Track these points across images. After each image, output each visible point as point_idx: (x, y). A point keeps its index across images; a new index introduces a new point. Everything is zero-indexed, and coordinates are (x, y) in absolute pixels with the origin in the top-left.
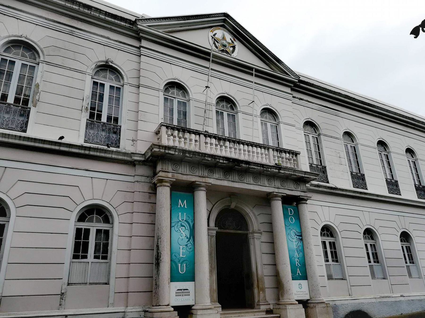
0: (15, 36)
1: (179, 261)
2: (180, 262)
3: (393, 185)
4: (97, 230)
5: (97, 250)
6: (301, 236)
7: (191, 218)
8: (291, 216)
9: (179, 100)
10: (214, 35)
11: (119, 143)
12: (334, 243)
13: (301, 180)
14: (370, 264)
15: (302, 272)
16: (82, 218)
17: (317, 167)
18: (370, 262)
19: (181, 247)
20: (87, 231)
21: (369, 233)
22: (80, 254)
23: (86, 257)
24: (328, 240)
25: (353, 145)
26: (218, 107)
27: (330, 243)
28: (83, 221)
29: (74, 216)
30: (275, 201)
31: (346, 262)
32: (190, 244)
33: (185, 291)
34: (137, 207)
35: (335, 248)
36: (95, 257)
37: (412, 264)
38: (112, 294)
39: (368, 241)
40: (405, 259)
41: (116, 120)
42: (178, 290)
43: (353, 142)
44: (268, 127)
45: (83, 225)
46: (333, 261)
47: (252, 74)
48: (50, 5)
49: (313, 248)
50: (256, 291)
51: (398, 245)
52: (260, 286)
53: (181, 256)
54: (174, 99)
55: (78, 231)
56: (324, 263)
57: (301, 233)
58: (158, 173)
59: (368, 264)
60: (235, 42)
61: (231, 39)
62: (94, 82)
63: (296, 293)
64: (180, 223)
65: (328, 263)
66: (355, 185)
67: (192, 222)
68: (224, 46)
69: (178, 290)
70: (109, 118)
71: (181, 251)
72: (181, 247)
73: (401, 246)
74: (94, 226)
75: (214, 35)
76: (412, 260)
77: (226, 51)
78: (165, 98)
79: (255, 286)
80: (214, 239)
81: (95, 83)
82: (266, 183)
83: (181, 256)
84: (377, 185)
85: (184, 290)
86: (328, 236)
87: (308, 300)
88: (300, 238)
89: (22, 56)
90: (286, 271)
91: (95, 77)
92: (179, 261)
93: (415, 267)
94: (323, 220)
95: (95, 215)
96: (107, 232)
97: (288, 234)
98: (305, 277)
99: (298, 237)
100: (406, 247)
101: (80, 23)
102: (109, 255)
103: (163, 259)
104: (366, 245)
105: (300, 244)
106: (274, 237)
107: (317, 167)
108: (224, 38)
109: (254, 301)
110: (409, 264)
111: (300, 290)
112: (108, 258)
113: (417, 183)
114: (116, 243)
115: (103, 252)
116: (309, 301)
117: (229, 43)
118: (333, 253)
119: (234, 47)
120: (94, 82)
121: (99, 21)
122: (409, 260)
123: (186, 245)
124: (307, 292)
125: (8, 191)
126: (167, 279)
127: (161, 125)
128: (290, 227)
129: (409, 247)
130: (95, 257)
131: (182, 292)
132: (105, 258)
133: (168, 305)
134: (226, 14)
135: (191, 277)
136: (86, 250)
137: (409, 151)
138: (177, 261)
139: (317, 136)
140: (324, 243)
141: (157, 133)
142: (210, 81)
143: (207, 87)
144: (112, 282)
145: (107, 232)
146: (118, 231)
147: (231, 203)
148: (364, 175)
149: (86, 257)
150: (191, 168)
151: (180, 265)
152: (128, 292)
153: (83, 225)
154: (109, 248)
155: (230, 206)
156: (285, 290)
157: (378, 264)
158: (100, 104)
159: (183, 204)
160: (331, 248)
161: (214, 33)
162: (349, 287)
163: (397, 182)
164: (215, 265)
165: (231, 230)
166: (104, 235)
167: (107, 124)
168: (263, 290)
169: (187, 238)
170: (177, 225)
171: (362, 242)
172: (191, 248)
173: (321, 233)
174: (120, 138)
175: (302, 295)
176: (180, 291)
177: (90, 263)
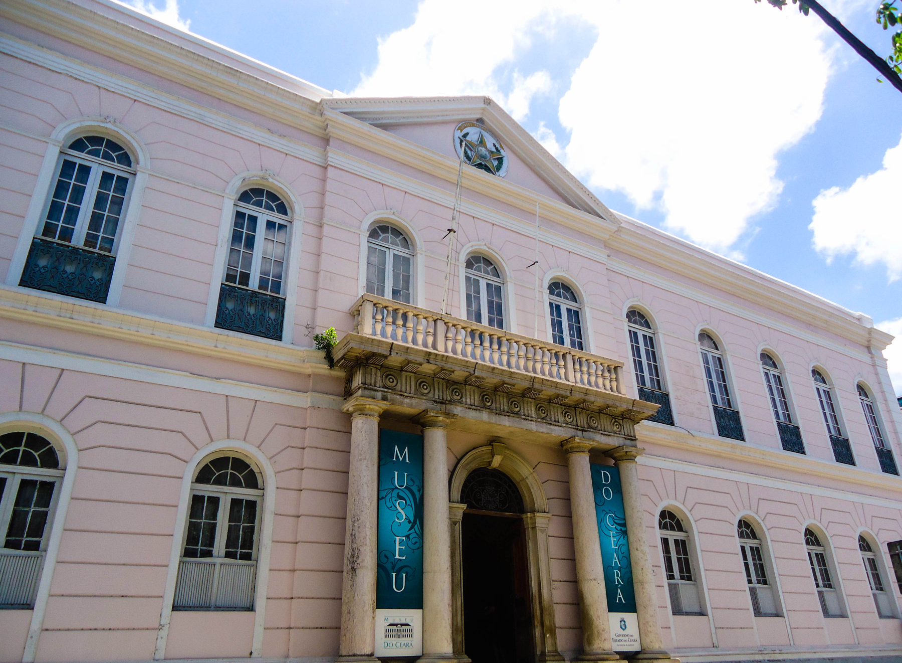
1: (393, 568)
2: (397, 568)
4: (22, 480)
5: (231, 542)
6: (624, 525)
7: (417, 482)
8: (605, 485)
9: (396, 253)
10: (465, 136)
11: (281, 331)
12: (683, 542)
13: (625, 417)
14: (751, 585)
15: (623, 597)
16: (203, 476)
18: (750, 582)
19: (397, 538)
20: (214, 502)
22: (199, 547)
23: (209, 554)
24: (673, 536)
25: (648, 334)
26: (470, 271)
27: (676, 541)
28: (207, 481)
29: (190, 472)
30: (577, 454)
31: (706, 578)
32: (414, 535)
33: (404, 627)
34: (310, 458)
36: (228, 555)
38: (259, 630)
41: (277, 286)
42: (390, 625)
43: (717, 349)
44: (562, 312)
45: (208, 490)
49: (645, 548)
50: (538, 632)
51: (859, 556)
52: (547, 622)
53: (397, 557)
54: (387, 250)
55: (197, 500)
56: (665, 582)
57: (625, 519)
58: (356, 391)
59: (747, 586)
60: (502, 151)
61: (494, 145)
62: (237, 212)
63: (615, 638)
64: (396, 492)
65: (672, 581)
67: (419, 491)
68: (483, 157)
69: (390, 625)
70: (263, 284)
71: (398, 547)
72: (397, 538)
74: (227, 494)
75: (465, 136)
76: (829, 580)
77: (486, 166)
78: (369, 247)
79: (536, 623)
80: (459, 527)
81: (240, 215)
83: (397, 557)
85: (402, 625)
86: (672, 529)
87: (637, 653)
88: (623, 529)
89: (266, 208)
90: (596, 593)
91: (242, 204)
92: (393, 568)
93: (833, 594)
95: (230, 471)
96: (252, 506)
97: (600, 522)
98: (630, 606)
99: (619, 528)
100: (816, 554)
102: (254, 551)
103: (363, 561)
104: (743, 548)
105: (622, 541)
106: (575, 526)
108: (482, 142)
109: (534, 653)
110: (677, 580)
111: (621, 632)
112: (42, 546)
113: (720, 404)
114: (269, 528)
115: (243, 545)
116: (640, 656)
117: (492, 152)
118: (681, 563)
119: (500, 160)
120: (237, 212)
123: (408, 536)
124: (636, 636)
125: (66, 416)
126: (371, 602)
127: (363, 300)
128: (603, 508)
129: (822, 555)
130: (228, 555)
131: (399, 629)
132: (247, 557)
133: (372, 655)
134: (488, 99)
135: (414, 598)
136: (210, 541)
138: (388, 566)
139: (651, 335)
140: (665, 541)
141: (356, 313)
142: (457, 220)
143: (450, 230)
144: (261, 604)
145: (252, 506)
146: (273, 503)
147: (493, 457)
148: (738, 412)
149: (209, 554)
150: (386, 377)
151: (394, 574)
152: (290, 628)
153: (208, 490)
154: (255, 537)
155: (490, 463)
156: (595, 631)
158: (247, 255)
161: (465, 131)
162: (713, 630)
163: (797, 428)
164: (460, 575)
165: (491, 510)
166: (246, 513)
167: (84, 250)
168: (552, 631)
169: (409, 522)
170: (389, 497)
171: (737, 542)
172: (416, 543)
173: (660, 523)
174: (282, 321)
175: (628, 643)
176: (394, 627)
177: (218, 566)
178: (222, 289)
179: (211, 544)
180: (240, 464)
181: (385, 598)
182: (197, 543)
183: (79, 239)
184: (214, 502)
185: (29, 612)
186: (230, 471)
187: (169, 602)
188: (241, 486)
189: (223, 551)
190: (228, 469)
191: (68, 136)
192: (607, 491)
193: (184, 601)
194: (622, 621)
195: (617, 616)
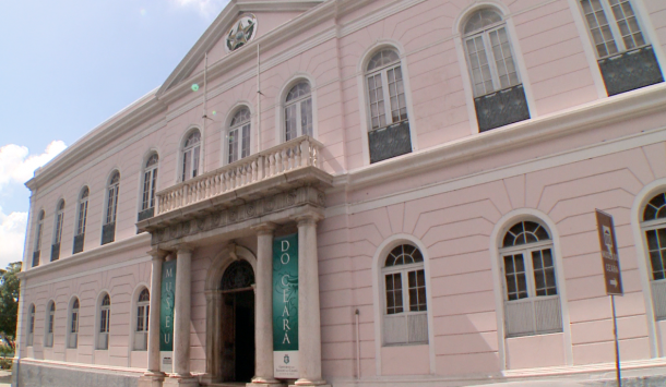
36: (412, 309)
95: (524, 232)
130: (412, 309)
136: (400, 302)
178: (600, 66)
179: (401, 304)
180: (531, 225)
181: (278, 345)
182: (515, 288)
183: (621, 47)
184: (398, 276)
185: (425, 346)
186: (524, 232)
187: (378, 342)
188: (535, 240)
189: (535, 293)
190: (525, 229)
191: (460, 30)
192: (285, 257)
193: (390, 341)
194: (287, 356)
195: (280, 354)
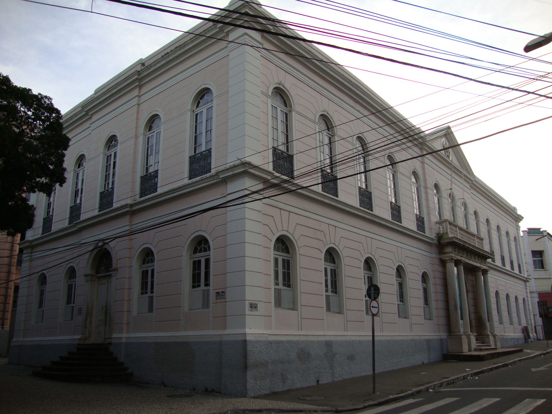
0: (284, 87)
3: (396, 210)
17: (282, 154)
21: (283, 244)
35: (289, 269)
37: (285, 288)
39: (328, 264)
40: (327, 286)
46: (284, 285)
47: (461, 177)
48: (311, 64)
66: (362, 203)
73: (363, 274)
82: (465, 256)
84: (381, 210)
94: (280, 228)
101: (321, 80)
107: (282, 154)
110: (329, 293)
121: (332, 79)
122: (332, 288)
137: (280, 93)
157: (288, 288)
159: (470, 277)
160: (284, 267)
171: (322, 264)
